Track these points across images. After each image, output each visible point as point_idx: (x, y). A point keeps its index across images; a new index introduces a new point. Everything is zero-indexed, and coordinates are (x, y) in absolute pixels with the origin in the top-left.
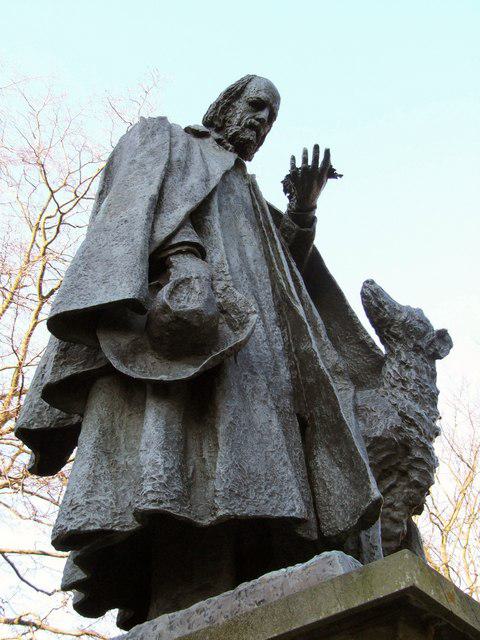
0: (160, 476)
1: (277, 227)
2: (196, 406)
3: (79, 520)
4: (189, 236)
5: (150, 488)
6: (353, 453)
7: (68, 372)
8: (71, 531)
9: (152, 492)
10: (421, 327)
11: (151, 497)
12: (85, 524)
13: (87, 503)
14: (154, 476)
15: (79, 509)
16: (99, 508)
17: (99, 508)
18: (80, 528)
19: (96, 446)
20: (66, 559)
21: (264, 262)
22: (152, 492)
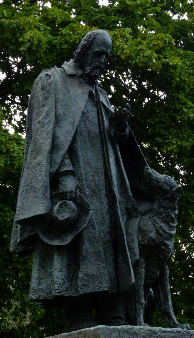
0: (60, 283)
1: (129, 252)
2: (73, 255)
3: (36, 295)
4: (68, 167)
5: (57, 288)
6: (103, 106)
7: (26, 235)
8: (34, 299)
9: (57, 289)
10: (156, 169)
11: (57, 291)
12: (38, 297)
13: (38, 289)
14: (58, 283)
15: (36, 291)
16: (42, 291)
17: (42, 291)
18: (37, 298)
19: (39, 266)
20: (62, 66)
21: (98, 125)
22: (57, 289)
